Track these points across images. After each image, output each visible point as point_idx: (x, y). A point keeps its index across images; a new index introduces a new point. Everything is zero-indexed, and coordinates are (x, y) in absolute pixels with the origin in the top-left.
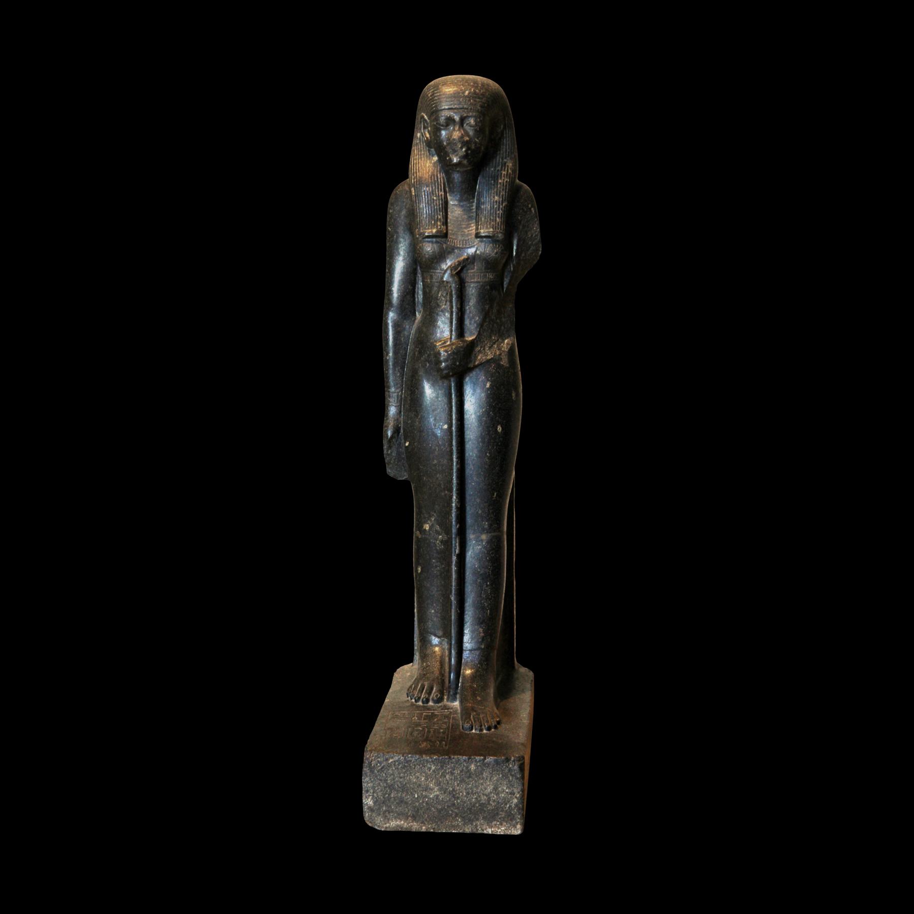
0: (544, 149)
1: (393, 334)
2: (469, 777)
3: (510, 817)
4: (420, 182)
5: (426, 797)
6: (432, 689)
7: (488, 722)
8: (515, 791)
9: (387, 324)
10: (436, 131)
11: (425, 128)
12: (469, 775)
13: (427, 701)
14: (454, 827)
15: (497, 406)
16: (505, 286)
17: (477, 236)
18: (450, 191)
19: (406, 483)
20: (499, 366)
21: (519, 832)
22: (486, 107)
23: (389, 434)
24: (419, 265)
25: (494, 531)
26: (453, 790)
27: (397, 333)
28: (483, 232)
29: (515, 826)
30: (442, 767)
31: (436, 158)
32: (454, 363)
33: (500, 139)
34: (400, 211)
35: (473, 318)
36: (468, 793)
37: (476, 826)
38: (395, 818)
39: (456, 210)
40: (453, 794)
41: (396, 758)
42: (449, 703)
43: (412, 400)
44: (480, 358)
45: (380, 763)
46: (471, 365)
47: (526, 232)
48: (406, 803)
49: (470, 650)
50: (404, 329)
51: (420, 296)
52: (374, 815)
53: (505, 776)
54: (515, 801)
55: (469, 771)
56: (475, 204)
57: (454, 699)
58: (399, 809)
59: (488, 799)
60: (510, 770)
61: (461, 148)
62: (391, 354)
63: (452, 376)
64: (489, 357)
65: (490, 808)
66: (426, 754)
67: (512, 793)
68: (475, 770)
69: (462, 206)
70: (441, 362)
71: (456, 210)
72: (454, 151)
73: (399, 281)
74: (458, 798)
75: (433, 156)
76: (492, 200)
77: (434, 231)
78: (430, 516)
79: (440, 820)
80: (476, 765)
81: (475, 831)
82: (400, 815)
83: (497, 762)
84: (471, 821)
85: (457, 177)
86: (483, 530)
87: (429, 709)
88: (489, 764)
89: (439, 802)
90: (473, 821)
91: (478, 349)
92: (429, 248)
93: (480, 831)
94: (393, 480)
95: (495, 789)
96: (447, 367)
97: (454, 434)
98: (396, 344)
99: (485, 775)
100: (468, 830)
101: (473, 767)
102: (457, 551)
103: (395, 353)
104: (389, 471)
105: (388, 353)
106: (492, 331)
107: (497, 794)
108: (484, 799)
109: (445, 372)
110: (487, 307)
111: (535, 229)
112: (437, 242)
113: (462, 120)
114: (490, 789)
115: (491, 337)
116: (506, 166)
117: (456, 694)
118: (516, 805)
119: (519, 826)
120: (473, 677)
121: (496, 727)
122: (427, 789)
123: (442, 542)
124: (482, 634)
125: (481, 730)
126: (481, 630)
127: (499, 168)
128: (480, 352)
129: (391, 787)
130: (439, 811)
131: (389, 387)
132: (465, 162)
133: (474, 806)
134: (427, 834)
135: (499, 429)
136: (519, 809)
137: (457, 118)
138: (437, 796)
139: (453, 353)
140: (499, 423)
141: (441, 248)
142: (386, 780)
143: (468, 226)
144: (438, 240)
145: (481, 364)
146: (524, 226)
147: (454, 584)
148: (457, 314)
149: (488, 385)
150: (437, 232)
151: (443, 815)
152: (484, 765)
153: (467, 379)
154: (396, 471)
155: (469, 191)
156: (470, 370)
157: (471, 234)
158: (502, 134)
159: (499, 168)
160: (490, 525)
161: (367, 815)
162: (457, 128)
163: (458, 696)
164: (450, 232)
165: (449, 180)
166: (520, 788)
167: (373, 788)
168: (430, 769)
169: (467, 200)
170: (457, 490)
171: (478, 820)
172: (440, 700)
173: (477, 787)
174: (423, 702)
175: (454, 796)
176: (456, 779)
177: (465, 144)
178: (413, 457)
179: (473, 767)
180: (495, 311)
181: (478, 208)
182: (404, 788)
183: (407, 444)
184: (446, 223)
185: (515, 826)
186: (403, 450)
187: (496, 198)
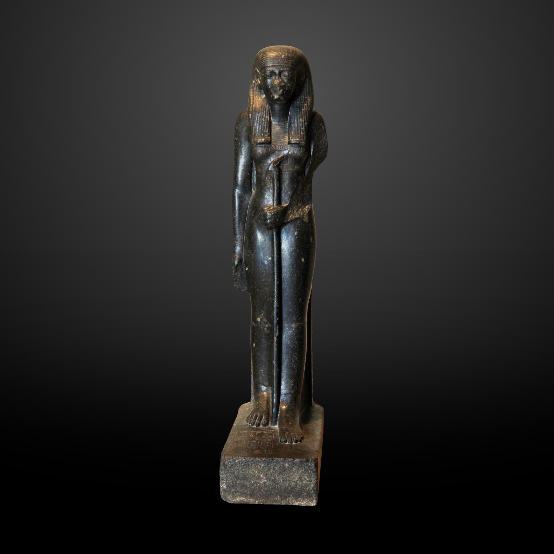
1: (238, 203)
2: (285, 471)
3: (309, 495)
4: (255, 111)
5: (258, 483)
6: (262, 417)
7: (295, 437)
8: (312, 479)
11: (257, 77)
12: (285, 469)
13: (259, 425)
14: (275, 501)
16: (306, 173)
17: (289, 143)
18: (273, 116)
20: (303, 222)
21: (315, 504)
25: (300, 322)
26: (275, 479)
27: (241, 202)
28: (293, 141)
29: (312, 501)
30: (268, 465)
31: (264, 96)
32: (275, 220)
33: (303, 84)
34: (243, 128)
35: (287, 192)
36: (284, 481)
37: (289, 500)
38: (240, 496)
39: (276, 127)
40: (275, 481)
41: (240, 460)
42: (272, 426)
43: (250, 242)
44: (291, 217)
45: (231, 462)
46: (286, 221)
47: (319, 141)
48: (246, 487)
49: (285, 394)
50: (245, 199)
51: (254, 180)
52: (227, 494)
53: (306, 471)
54: (312, 485)
55: (284, 467)
56: (288, 124)
57: (275, 424)
58: (242, 490)
59: (296, 485)
60: (309, 467)
61: (280, 90)
62: (237, 215)
63: (274, 228)
64: (296, 217)
65: (297, 489)
66: (258, 457)
67: (311, 481)
68: (288, 467)
69: (280, 125)
70: (267, 220)
71: (276, 127)
72: (275, 92)
74: (278, 484)
75: (262, 94)
77: (263, 140)
78: (261, 313)
79: (267, 497)
80: (288, 464)
81: (288, 504)
82: (243, 494)
83: (301, 462)
84: (285, 498)
85: (277, 107)
86: (293, 321)
87: (260, 430)
88: (296, 463)
89: (266, 486)
90: (287, 497)
91: (290, 211)
92: (260, 150)
93: (291, 504)
95: (300, 478)
96: (271, 223)
97: (275, 263)
98: (240, 209)
99: (294, 470)
100: (284, 503)
101: (287, 465)
102: (277, 334)
106: (298, 200)
107: (302, 481)
108: (293, 484)
109: (270, 225)
110: (295, 186)
112: (265, 147)
113: (280, 73)
114: (297, 478)
115: (297, 204)
117: (276, 420)
118: (313, 488)
119: (314, 501)
120: (287, 410)
121: (300, 441)
122: (259, 478)
123: (268, 328)
124: (292, 385)
125: (292, 443)
126: (292, 382)
127: (303, 102)
128: (291, 213)
129: (237, 477)
130: (266, 492)
132: (282, 98)
133: (287, 488)
134: (259, 506)
135: (303, 260)
136: (315, 490)
137: (277, 72)
138: (265, 482)
139: (275, 214)
140: (302, 256)
141: (267, 150)
142: (234, 473)
143: (284, 137)
144: (266, 145)
145: (291, 221)
146: (318, 137)
147: (275, 354)
148: (277, 190)
149: (296, 233)
150: (265, 141)
151: (268, 494)
152: (294, 463)
153: (283, 230)
155: (284, 116)
156: (285, 224)
157: (285, 142)
158: (304, 81)
159: (303, 102)
160: (297, 319)
161: (222, 494)
162: (277, 78)
163: (278, 422)
164: (273, 140)
165: (272, 109)
166: (315, 478)
167: (226, 477)
168: (261, 466)
169: (283, 121)
170: (277, 297)
171: (289, 497)
172: (267, 424)
173: (289, 477)
174: (256, 426)
175: (275, 482)
176: (276, 472)
177: (282, 87)
179: (287, 465)
180: (300, 188)
181: (290, 126)
182: (245, 478)
183: (247, 269)
184: (270, 135)
185: (312, 501)
186: (244, 273)
187: (301, 120)
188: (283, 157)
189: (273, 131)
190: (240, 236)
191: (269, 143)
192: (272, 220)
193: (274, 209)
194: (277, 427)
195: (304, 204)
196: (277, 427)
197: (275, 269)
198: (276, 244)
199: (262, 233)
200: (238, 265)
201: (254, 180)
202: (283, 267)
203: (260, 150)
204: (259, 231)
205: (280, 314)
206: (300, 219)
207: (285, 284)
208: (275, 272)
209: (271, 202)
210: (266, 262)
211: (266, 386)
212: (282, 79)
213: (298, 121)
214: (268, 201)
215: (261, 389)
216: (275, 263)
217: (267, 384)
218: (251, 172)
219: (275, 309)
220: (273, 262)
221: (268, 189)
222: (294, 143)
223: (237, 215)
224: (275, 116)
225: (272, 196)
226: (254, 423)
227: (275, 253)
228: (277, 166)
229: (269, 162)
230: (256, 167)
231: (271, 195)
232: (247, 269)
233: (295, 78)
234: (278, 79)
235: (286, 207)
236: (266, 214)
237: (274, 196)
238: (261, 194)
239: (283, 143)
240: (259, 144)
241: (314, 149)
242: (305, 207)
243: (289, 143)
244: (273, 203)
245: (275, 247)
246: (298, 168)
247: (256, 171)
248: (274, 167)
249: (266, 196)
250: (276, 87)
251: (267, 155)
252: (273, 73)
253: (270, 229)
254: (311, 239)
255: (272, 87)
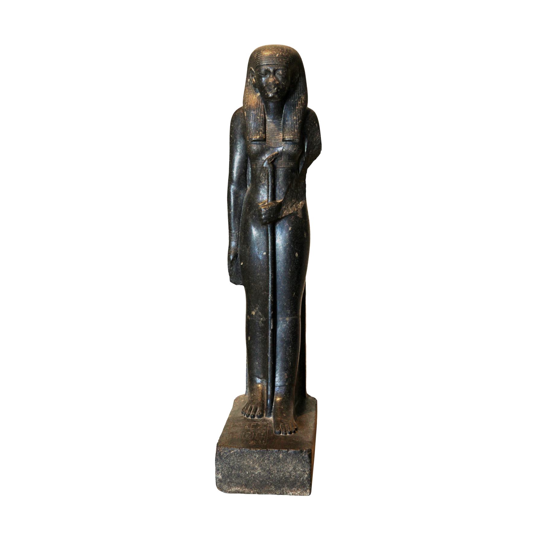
1: (234, 199)
2: (279, 462)
5: (253, 473)
6: (257, 409)
7: (290, 429)
8: (306, 470)
11: (252, 76)
12: (279, 460)
13: (254, 416)
16: (300, 170)
17: (284, 140)
18: (267, 114)
20: (297, 218)
25: (294, 316)
26: (269, 469)
28: (287, 138)
30: (263, 456)
31: (259, 94)
32: (270, 216)
33: (297, 82)
34: (238, 125)
35: (281, 189)
36: (278, 471)
38: (235, 486)
39: (271, 125)
40: (269, 472)
41: (235, 450)
42: (267, 418)
43: (245, 238)
44: (285, 213)
45: (226, 453)
46: (280, 217)
47: (313, 138)
48: (241, 477)
49: (279, 386)
50: (240, 195)
51: (249, 176)
52: (222, 484)
53: (300, 461)
54: (306, 476)
55: (279, 458)
56: (282, 121)
57: (270, 415)
58: (237, 481)
60: (303, 457)
61: (274, 88)
62: (232, 211)
63: (269, 223)
64: (290, 212)
65: (291, 480)
66: (253, 448)
67: (304, 471)
68: (282, 458)
69: (274, 123)
70: (262, 215)
71: (271, 125)
72: (270, 90)
73: (237, 167)
74: (272, 474)
75: (257, 93)
77: (258, 137)
78: (256, 307)
79: (261, 487)
80: (283, 455)
83: (295, 453)
85: (271, 105)
86: (287, 315)
87: (255, 421)
88: (290, 454)
89: (261, 477)
90: (281, 488)
91: (284, 207)
92: (255, 147)
95: (294, 469)
96: (265, 218)
97: (270, 258)
99: (288, 460)
101: (281, 456)
102: (272, 328)
106: (292, 196)
107: (296, 472)
108: (287, 474)
109: (265, 221)
110: (289, 182)
112: (259, 144)
113: (275, 71)
114: (291, 469)
115: (291, 200)
117: (271, 412)
120: (281, 402)
121: (294, 432)
122: (254, 469)
123: (262, 322)
124: (286, 377)
125: (286, 434)
126: (286, 374)
127: (297, 100)
128: (285, 209)
129: (232, 468)
130: (261, 482)
132: (276, 96)
133: (282, 479)
135: (297, 255)
137: (271, 70)
138: (260, 473)
139: (269, 210)
140: (296, 251)
141: (262, 147)
142: (229, 464)
143: (278, 134)
144: (260, 142)
145: (286, 216)
146: (311, 135)
147: (269, 347)
148: (272, 186)
149: (290, 229)
150: (260, 138)
152: (288, 454)
153: (278, 225)
155: (278, 113)
156: (279, 220)
157: (280, 139)
158: (298, 80)
159: (297, 100)
160: (291, 312)
162: (271, 76)
163: (272, 414)
164: (267, 138)
165: (267, 107)
167: (222, 468)
168: (255, 457)
169: (278, 119)
170: (272, 291)
171: (284, 487)
172: (261, 416)
173: (283, 468)
174: (251, 417)
175: (269, 473)
176: (271, 463)
177: (276, 85)
179: (281, 456)
180: (294, 185)
181: (284, 123)
182: (240, 468)
183: (242, 264)
184: (265, 133)
186: (239, 267)
187: (295, 118)
188: (278, 154)
189: (267, 128)
190: (236, 231)
191: (263, 140)
192: (267, 215)
193: (269, 204)
194: (271, 418)
196: (271, 418)
197: (270, 263)
198: (271, 240)
199: (257, 229)
200: (233, 260)
201: (249, 176)
202: (277, 261)
203: (255, 147)
204: (254, 226)
205: (274, 308)
206: (294, 214)
207: (279, 279)
208: (270, 266)
209: (265, 198)
210: (261, 257)
211: (261, 379)
212: (276, 77)
213: (292, 119)
214: (263, 197)
215: (255, 381)
216: (270, 258)
217: (262, 376)
218: (246, 168)
219: (270, 303)
220: (268, 257)
221: (263, 185)
222: (288, 141)
223: (232, 211)
224: (269, 114)
225: (266, 192)
226: (249, 415)
227: (270, 248)
228: (271, 162)
229: (264, 158)
230: (251, 163)
231: (266, 191)
232: (242, 264)
233: (289, 77)
234: (273, 77)
235: (281, 203)
236: (261, 210)
237: (268, 192)
238: (255, 191)
239: (278, 140)
240: (254, 141)
241: (307, 146)
242: (299, 202)
243: (284, 140)
244: (268, 199)
245: (270, 242)
246: (292, 164)
247: (251, 167)
248: (268, 164)
249: (261, 192)
250: (271, 86)
251: (262, 152)
252: (267, 72)
253: (265, 224)
254: (305, 234)
255: (266, 86)
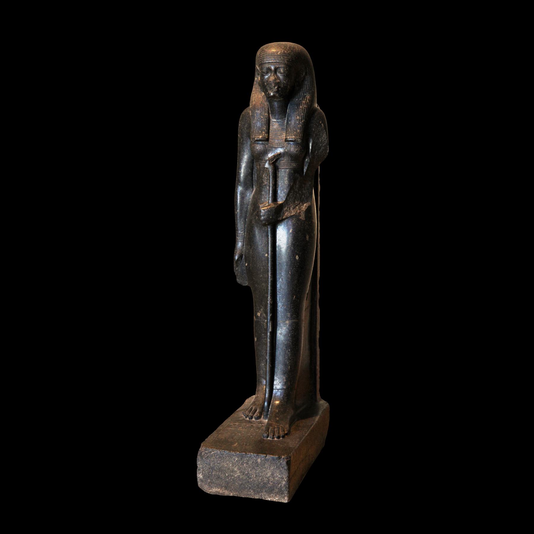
0: (335, 87)
2: (257, 466)
3: (280, 492)
4: (254, 108)
5: (232, 476)
6: (256, 411)
7: (279, 433)
8: (284, 477)
9: (237, 193)
10: (262, 76)
13: (252, 418)
15: (299, 242)
16: (305, 171)
18: (272, 113)
19: (248, 288)
20: (299, 220)
21: (286, 502)
22: (293, 64)
23: (236, 258)
24: (256, 158)
25: (294, 319)
26: (248, 473)
27: (242, 198)
28: (290, 138)
29: (284, 498)
30: (241, 459)
32: (268, 217)
33: (303, 81)
34: (244, 125)
35: (283, 190)
36: (256, 476)
38: (215, 487)
39: (275, 124)
41: (216, 452)
43: (249, 238)
44: (287, 214)
46: (280, 219)
47: (318, 139)
48: (221, 479)
50: (246, 196)
51: (255, 177)
52: (203, 484)
53: (278, 468)
54: (284, 483)
55: (257, 462)
56: (286, 121)
58: (217, 482)
59: (268, 480)
61: (275, 87)
62: (238, 211)
63: (268, 225)
64: (292, 214)
65: (269, 485)
67: (282, 478)
70: (261, 216)
72: (271, 89)
76: (296, 119)
77: (261, 137)
78: (260, 308)
82: (219, 486)
83: (273, 459)
84: (258, 493)
85: (276, 104)
86: (287, 317)
87: (251, 423)
90: (259, 492)
94: (240, 286)
95: (272, 474)
96: (264, 220)
97: (269, 260)
98: (241, 205)
100: (257, 497)
101: (259, 460)
102: (270, 330)
103: (241, 210)
104: (238, 280)
105: (237, 210)
106: (295, 198)
107: (274, 478)
108: (266, 480)
109: (264, 222)
111: (324, 137)
112: (262, 144)
113: (276, 69)
114: (269, 474)
115: (294, 202)
116: (306, 98)
118: (285, 485)
119: (286, 498)
120: (278, 406)
121: (283, 437)
122: (233, 471)
125: (273, 438)
126: (284, 378)
128: (286, 210)
129: (212, 468)
131: (238, 230)
132: (277, 95)
133: (260, 484)
134: (233, 497)
135: (297, 257)
136: (286, 488)
137: (273, 68)
138: (239, 476)
139: (268, 211)
140: (297, 254)
142: (210, 464)
143: (281, 134)
144: (263, 142)
145: (287, 218)
146: (316, 135)
148: (273, 187)
152: (266, 460)
154: (242, 280)
155: (283, 113)
156: (283, 220)
158: (304, 78)
160: (292, 315)
161: (199, 484)
162: (272, 75)
164: (270, 137)
165: (271, 106)
166: (287, 475)
167: (203, 468)
168: (235, 459)
169: (281, 118)
170: (271, 293)
171: (262, 492)
172: (259, 417)
175: (248, 477)
176: (250, 467)
178: (250, 272)
179: (259, 460)
180: (297, 186)
181: (287, 123)
182: (220, 470)
184: (268, 132)
185: (284, 498)
186: (244, 268)
187: (298, 117)
189: (271, 129)
195: (303, 202)
242: (303, 204)
